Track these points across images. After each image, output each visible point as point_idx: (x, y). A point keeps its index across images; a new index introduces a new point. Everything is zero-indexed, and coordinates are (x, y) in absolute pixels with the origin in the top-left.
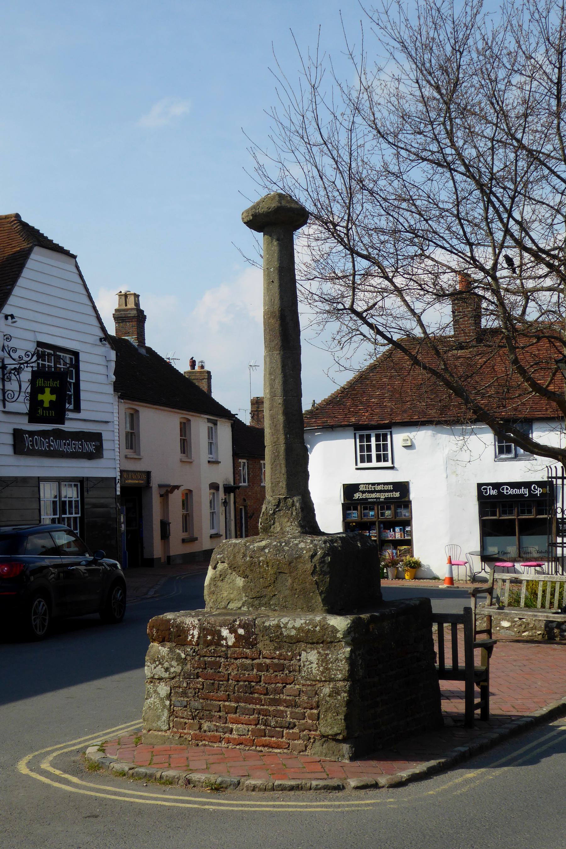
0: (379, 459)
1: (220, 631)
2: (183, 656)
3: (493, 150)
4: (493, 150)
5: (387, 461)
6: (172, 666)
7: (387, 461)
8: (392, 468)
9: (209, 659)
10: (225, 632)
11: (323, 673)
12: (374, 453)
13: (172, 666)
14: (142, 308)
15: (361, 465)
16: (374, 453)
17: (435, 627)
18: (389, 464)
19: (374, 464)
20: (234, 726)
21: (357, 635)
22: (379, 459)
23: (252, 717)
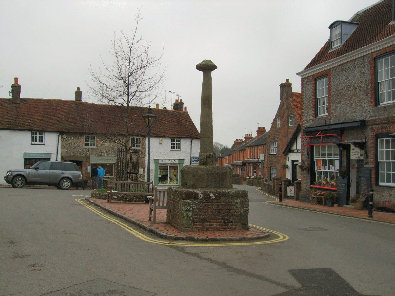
0: (40, 141)
1: (210, 195)
2: (197, 203)
3: (130, 59)
4: (130, 59)
5: (179, 149)
6: (193, 206)
7: (179, 149)
8: (44, 144)
9: (206, 203)
10: (211, 195)
11: (241, 205)
12: (38, 139)
13: (193, 206)
14: (19, 83)
15: (32, 143)
16: (38, 139)
17: (165, 205)
18: (43, 143)
19: (38, 143)
20: (214, 224)
21: (335, 184)
22: (177, 148)
23: (220, 220)
